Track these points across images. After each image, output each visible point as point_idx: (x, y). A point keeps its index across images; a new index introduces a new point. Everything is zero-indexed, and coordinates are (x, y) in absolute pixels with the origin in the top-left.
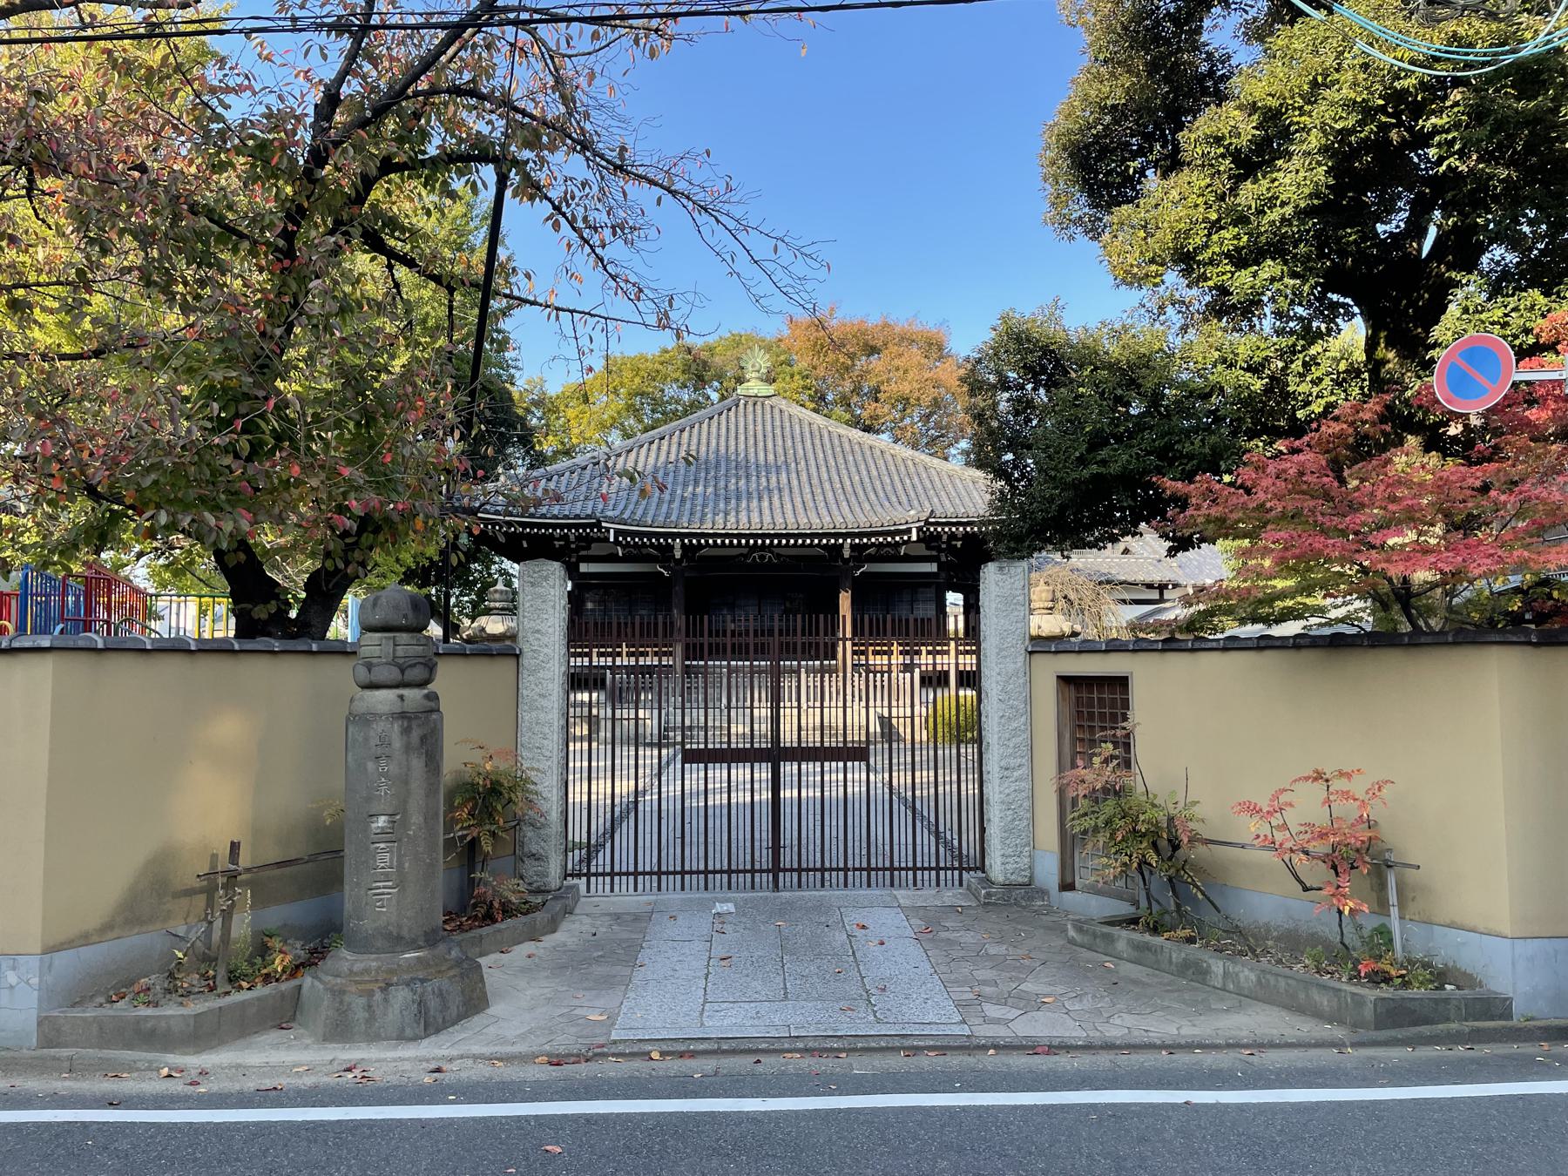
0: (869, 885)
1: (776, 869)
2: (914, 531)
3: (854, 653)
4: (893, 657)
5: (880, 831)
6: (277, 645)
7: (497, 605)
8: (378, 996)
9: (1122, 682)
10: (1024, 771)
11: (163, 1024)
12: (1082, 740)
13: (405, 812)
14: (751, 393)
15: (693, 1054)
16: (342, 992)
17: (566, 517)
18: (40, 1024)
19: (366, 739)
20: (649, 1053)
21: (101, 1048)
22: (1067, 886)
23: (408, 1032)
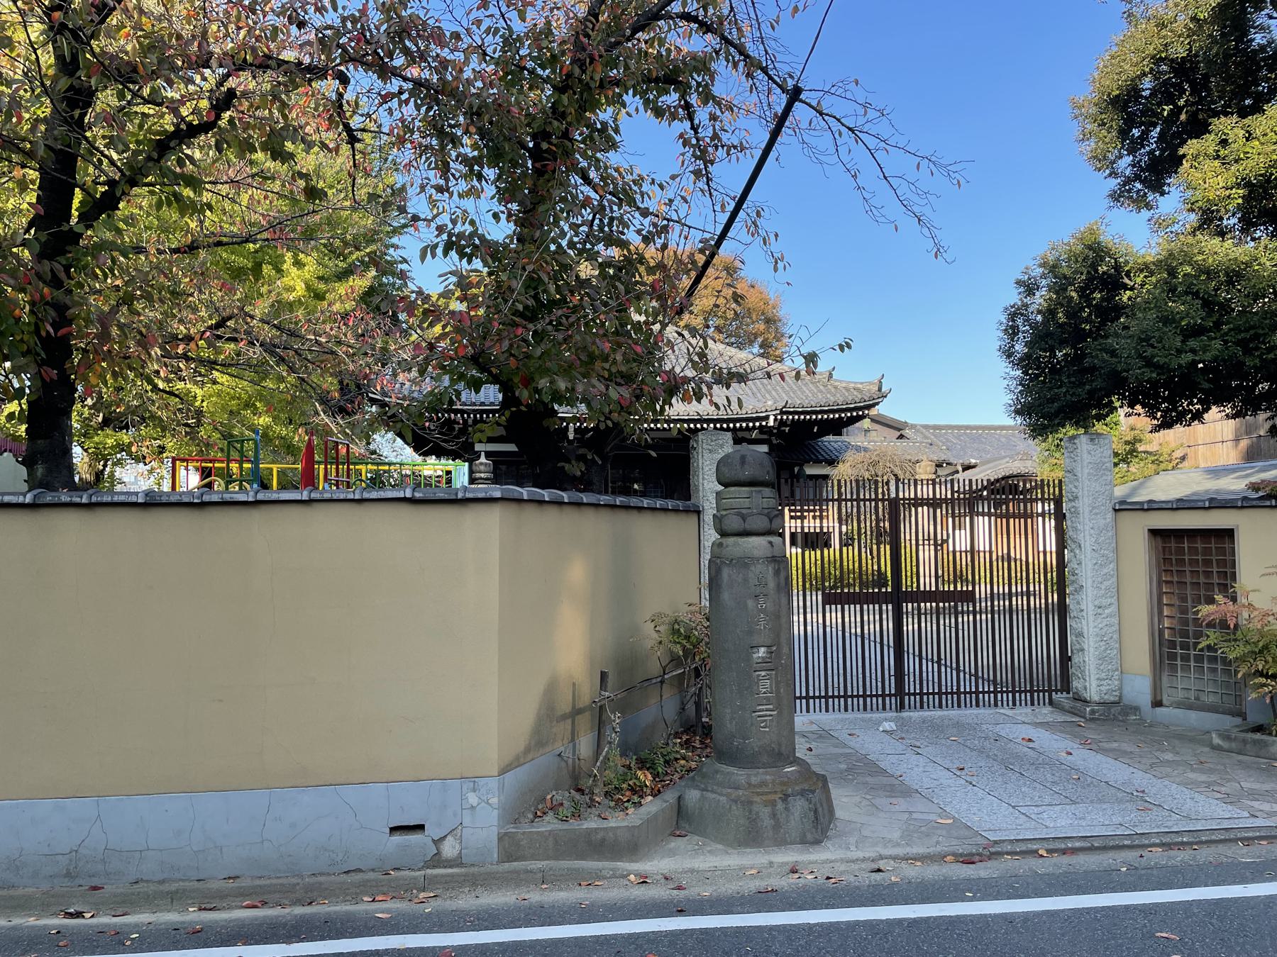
1: (900, 691)
2: (772, 418)
3: (791, 517)
4: (806, 521)
5: (854, 665)
7: (482, 475)
8: (780, 806)
9: (1228, 534)
10: (1113, 609)
11: (611, 834)
12: (1167, 582)
13: (779, 645)
15: (1074, 851)
16: (751, 803)
17: (474, 404)
19: (746, 580)
20: (1036, 851)
21: (557, 859)
22: (1157, 703)
23: (809, 837)
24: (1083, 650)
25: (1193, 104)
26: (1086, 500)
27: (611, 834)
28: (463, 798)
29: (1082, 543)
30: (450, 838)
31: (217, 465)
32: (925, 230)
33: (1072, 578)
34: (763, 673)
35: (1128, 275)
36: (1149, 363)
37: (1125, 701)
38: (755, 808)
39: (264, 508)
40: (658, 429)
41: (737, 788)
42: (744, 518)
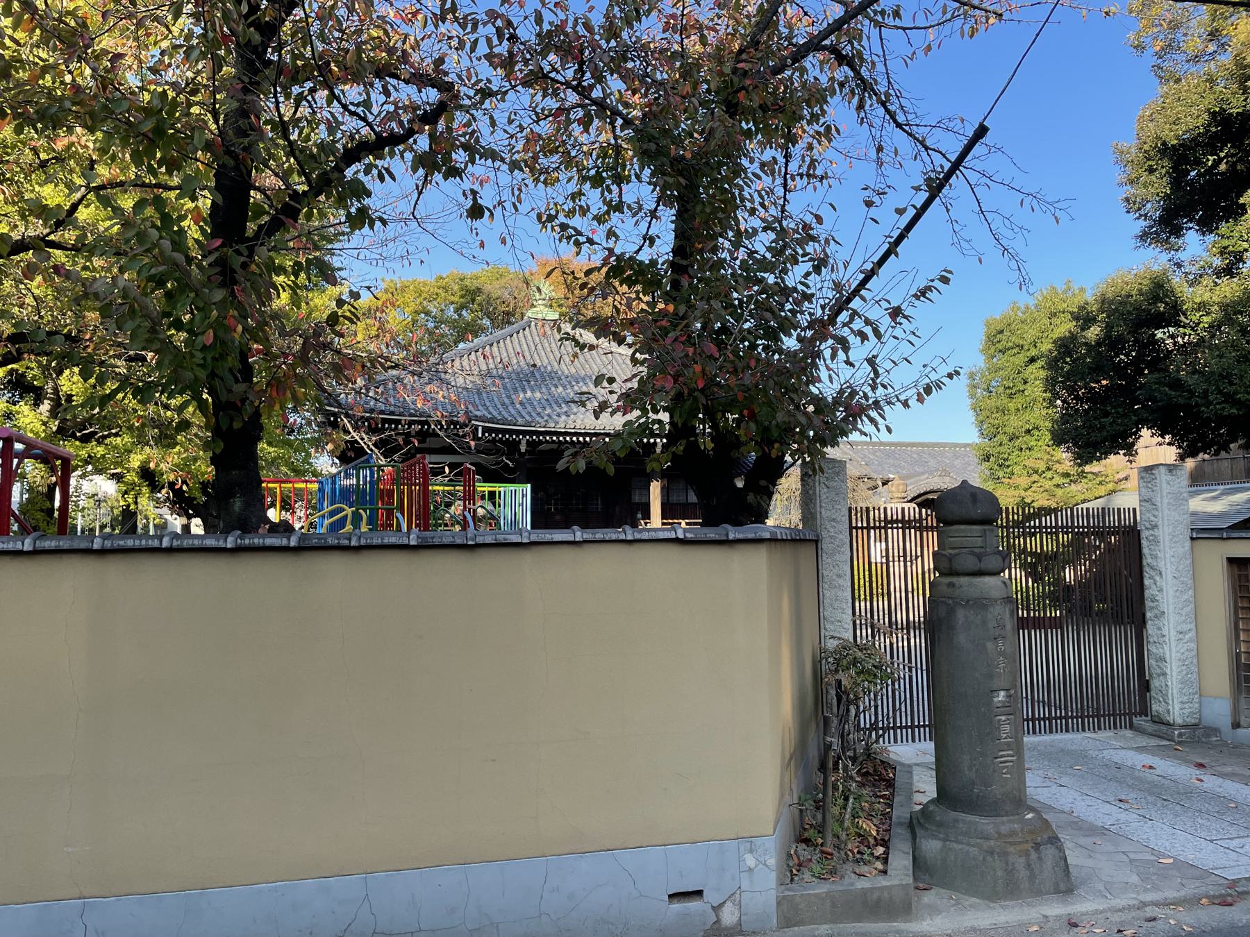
0: (1034, 732)
6: (579, 535)
8: (1033, 855)
12: (1243, 608)
14: (540, 316)
16: (1006, 854)
18: (779, 903)
19: (984, 623)
22: (1236, 725)
24: (1164, 674)
25: (1233, 155)
26: (1166, 528)
27: (886, 894)
28: (741, 860)
29: (1163, 570)
30: (729, 904)
31: (309, 486)
32: (1013, 264)
33: (1151, 604)
34: (1003, 718)
35: (1185, 314)
36: (1230, 399)
37: (1204, 723)
38: (1011, 859)
39: (535, 549)
40: (547, 442)
41: (987, 838)
42: (979, 557)
